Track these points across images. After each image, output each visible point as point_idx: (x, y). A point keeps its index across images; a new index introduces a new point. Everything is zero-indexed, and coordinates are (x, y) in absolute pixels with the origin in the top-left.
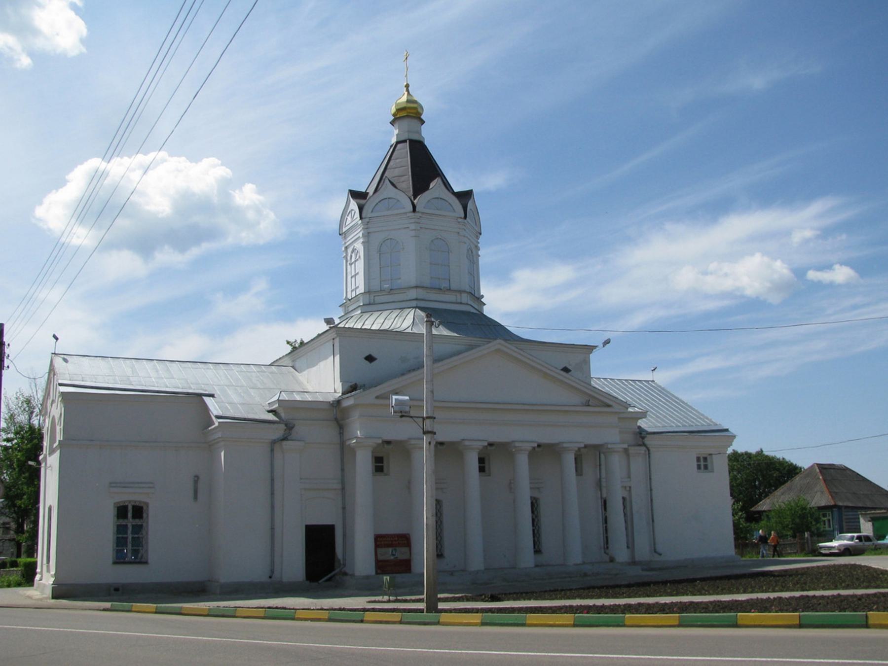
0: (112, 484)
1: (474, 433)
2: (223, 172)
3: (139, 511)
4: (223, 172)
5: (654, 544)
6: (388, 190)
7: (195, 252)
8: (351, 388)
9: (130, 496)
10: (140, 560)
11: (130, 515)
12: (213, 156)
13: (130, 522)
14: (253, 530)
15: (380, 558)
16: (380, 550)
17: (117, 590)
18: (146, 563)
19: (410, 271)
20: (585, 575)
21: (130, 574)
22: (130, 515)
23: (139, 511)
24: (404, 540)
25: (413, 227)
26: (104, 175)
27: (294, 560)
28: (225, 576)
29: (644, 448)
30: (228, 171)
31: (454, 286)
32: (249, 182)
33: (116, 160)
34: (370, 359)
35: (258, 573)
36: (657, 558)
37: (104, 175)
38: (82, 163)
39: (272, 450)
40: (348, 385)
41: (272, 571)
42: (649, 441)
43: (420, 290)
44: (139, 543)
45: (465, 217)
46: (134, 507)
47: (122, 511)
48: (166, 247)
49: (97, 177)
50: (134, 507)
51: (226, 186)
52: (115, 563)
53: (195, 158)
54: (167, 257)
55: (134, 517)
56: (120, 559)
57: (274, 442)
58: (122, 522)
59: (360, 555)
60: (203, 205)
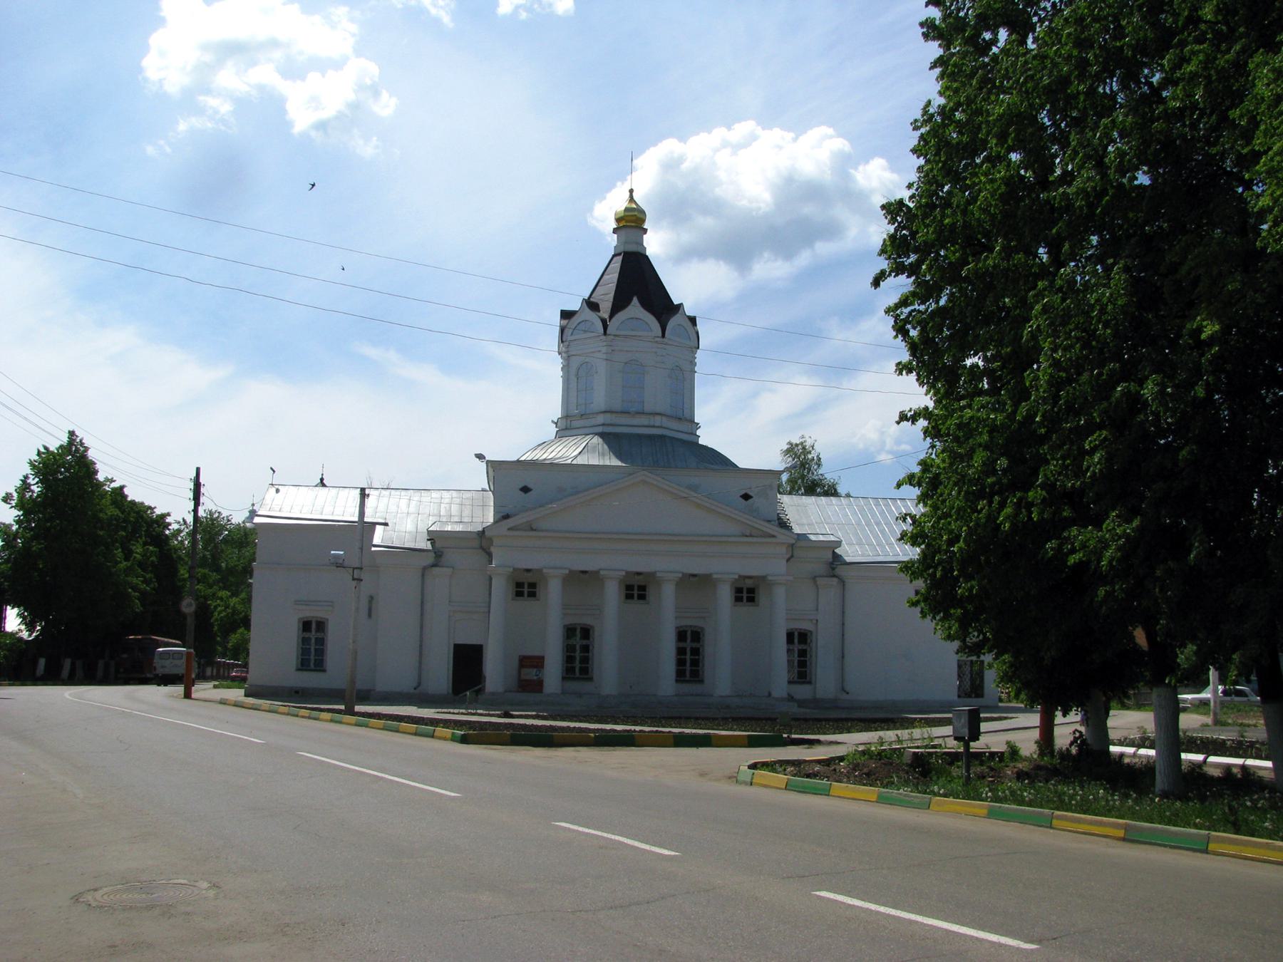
0: (297, 602)
1: (617, 563)
2: (841, 144)
3: (321, 625)
4: (841, 144)
5: (843, 681)
6: (589, 315)
7: (804, 259)
8: (503, 516)
9: (309, 613)
10: (320, 666)
11: (314, 626)
12: (820, 124)
13: (313, 635)
14: (403, 643)
15: (523, 677)
16: (525, 671)
17: (297, 692)
18: (324, 671)
19: (599, 399)
20: (728, 707)
21: (311, 680)
22: (314, 626)
23: (321, 625)
24: (536, 662)
25: (604, 350)
26: (681, 159)
27: (440, 674)
28: (381, 687)
29: (835, 580)
30: (846, 142)
31: (647, 408)
32: (882, 156)
33: (694, 140)
34: (525, 490)
35: (406, 684)
36: (844, 696)
37: (681, 159)
38: (655, 144)
39: (423, 575)
40: (500, 516)
41: (419, 684)
42: (840, 570)
43: (608, 415)
44: (321, 652)
45: (663, 336)
46: (582, 629)
47: (306, 626)
48: (766, 255)
49: (671, 165)
50: (582, 629)
51: (844, 163)
52: (298, 670)
53: (799, 127)
54: (769, 269)
55: (693, 641)
56: (304, 665)
57: (425, 569)
58: (681, 645)
59: (495, 671)
60: (813, 192)
